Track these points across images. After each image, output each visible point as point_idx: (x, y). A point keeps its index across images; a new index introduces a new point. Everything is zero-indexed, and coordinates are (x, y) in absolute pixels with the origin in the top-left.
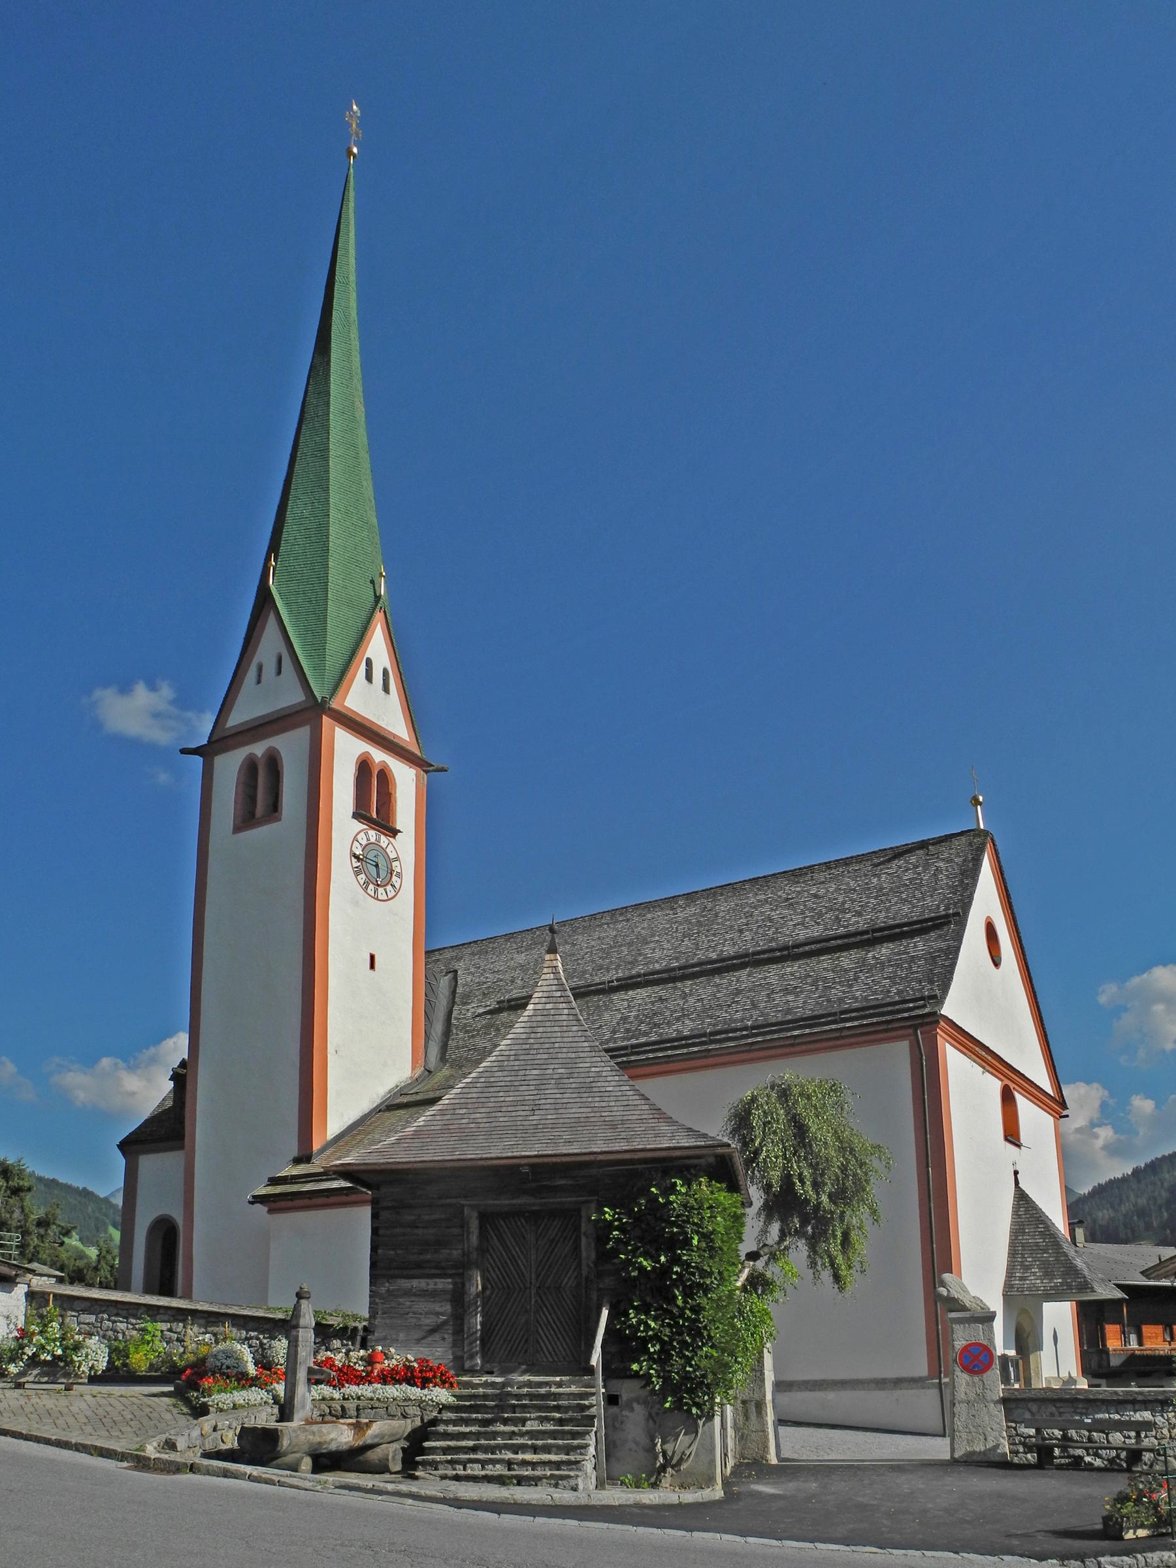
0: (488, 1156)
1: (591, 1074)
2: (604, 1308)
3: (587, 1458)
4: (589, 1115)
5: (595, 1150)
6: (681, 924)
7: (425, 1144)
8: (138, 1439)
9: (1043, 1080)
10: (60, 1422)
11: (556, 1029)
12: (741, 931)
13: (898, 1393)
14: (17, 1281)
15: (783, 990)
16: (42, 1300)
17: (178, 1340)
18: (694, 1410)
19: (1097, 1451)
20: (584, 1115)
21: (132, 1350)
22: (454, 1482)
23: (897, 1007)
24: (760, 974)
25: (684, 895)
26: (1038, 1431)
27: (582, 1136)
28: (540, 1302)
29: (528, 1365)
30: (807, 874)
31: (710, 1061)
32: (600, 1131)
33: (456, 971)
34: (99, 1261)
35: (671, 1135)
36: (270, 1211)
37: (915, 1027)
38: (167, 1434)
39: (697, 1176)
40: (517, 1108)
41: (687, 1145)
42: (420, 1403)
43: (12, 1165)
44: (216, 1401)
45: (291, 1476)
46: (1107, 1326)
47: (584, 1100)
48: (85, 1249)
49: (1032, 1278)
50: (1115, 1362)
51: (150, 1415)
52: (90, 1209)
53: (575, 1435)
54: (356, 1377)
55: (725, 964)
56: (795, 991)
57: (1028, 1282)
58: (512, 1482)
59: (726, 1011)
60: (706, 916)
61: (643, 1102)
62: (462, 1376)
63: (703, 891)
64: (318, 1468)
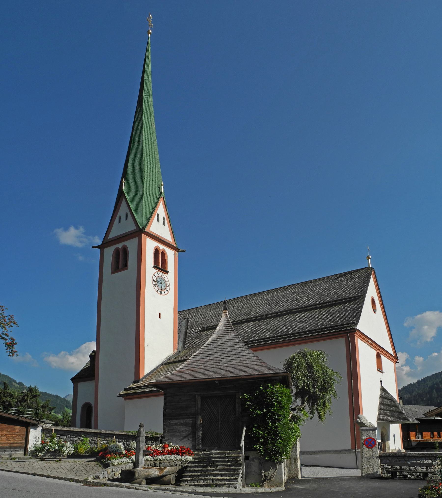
0: (204, 378)
1: (239, 350)
2: (244, 428)
3: (239, 477)
4: (239, 363)
5: (241, 375)
6: (266, 301)
7: (182, 375)
8: (86, 476)
9: (390, 350)
10: (58, 471)
11: (227, 335)
12: (286, 302)
13: (341, 455)
14: (38, 426)
15: (301, 322)
16: (47, 431)
17: (95, 443)
18: (276, 461)
19: (412, 473)
20: (237, 364)
21: (79, 447)
22: (194, 487)
23: (341, 327)
24: (293, 316)
25: (266, 291)
26: (392, 467)
27: (236, 370)
28: (222, 426)
29: (218, 447)
30: (309, 283)
31: (276, 345)
32: (243, 369)
33: (188, 318)
34: (63, 419)
35: (267, 369)
36: (125, 399)
37: (348, 333)
38: (96, 474)
39: (276, 383)
40: (214, 362)
41: (273, 372)
42: (181, 461)
43: (33, 388)
44: (112, 462)
45: (139, 486)
46: (410, 432)
47: (237, 358)
48: (56, 415)
49: (387, 416)
50: (413, 444)
51: (89, 467)
52: (58, 402)
53: (235, 470)
54: (159, 453)
55: (281, 313)
56: (305, 322)
57: (385, 418)
58: (214, 486)
59: (282, 329)
60: (274, 298)
61: (257, 359)
62: (195, 451)
63: (273, 289)
64: (147, 484)
